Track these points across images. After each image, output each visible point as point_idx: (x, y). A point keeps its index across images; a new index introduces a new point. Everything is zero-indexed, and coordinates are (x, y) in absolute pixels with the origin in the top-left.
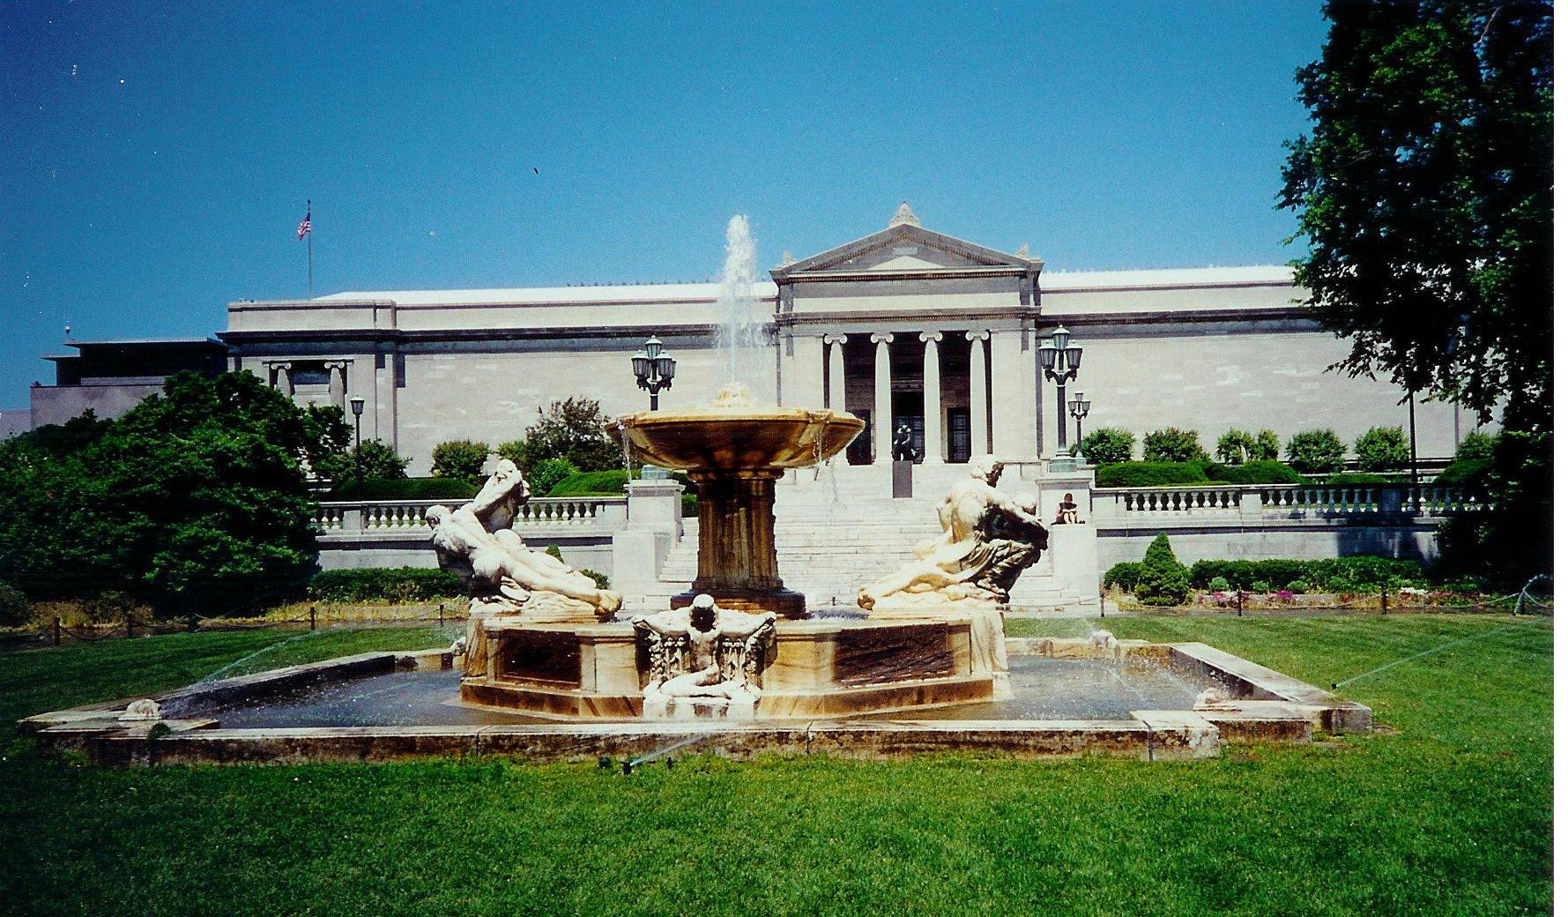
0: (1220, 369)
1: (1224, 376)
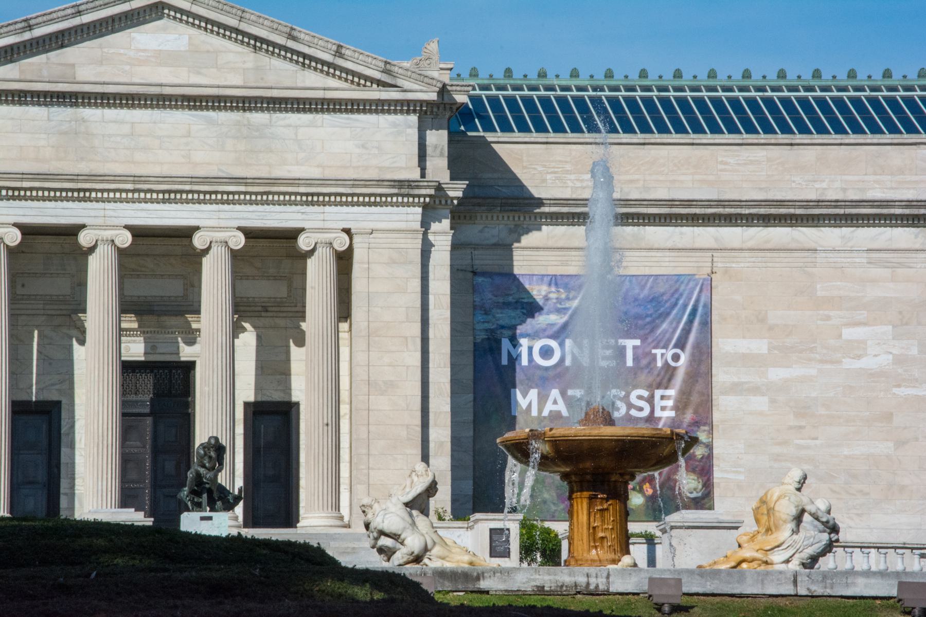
0: (849, 333)
1: (857, 349)
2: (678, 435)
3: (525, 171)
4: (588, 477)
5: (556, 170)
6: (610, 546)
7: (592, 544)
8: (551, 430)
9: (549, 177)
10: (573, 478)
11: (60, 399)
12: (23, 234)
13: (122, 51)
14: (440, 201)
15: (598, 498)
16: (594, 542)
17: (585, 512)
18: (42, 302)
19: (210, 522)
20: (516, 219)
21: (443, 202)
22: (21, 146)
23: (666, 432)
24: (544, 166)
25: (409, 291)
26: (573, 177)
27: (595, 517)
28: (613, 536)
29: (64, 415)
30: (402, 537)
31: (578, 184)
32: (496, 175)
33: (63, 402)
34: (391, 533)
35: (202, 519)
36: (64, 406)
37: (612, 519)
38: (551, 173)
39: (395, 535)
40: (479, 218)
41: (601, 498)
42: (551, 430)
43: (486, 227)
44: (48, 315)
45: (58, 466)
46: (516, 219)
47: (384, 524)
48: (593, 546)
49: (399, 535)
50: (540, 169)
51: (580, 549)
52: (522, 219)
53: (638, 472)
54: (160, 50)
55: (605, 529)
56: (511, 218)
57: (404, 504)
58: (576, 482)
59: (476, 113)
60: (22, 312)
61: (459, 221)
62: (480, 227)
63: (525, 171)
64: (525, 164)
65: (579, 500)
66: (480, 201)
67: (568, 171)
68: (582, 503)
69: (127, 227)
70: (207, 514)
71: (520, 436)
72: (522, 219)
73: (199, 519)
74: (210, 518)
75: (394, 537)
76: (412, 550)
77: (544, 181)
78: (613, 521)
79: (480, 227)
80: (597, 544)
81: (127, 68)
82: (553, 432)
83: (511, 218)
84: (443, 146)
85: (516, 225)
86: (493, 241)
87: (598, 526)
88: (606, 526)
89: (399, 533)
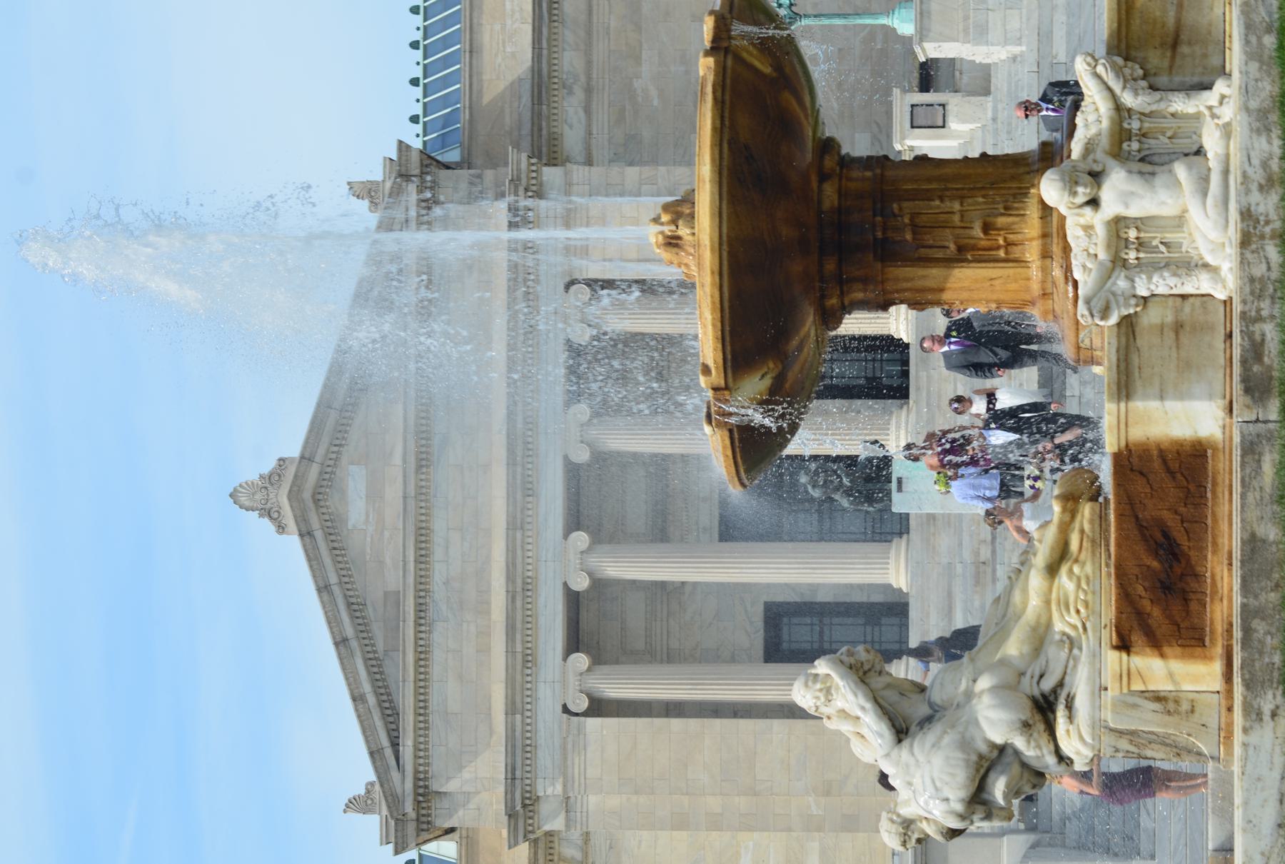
2: (716, 39)
3: (502, 77)
4: (830, 266)
5: (501, 41)
7: (1002, 253)
8: (706, 370)
9: (508, 50)
10: (833, 301)
13: (369, 539)
14: (533, 178)
15: (885, 240)
16: (998, 248)
20: (556, 86)
21: (534, 175)
22: (477, 652)
23: (709, 68)
24: (496, 55)
25: (636, 215)
26: (509, 22)
27: (931, 247)
29: (780, 599)
30: (983, 748)
31: (517, 15)
32: (507, 111)
34: (973, 780)
35: (900, 489)
38: (504, 47)
39: (978, 768)
40: (556, 130)
41: (884, 230)
42: (706, 370)
43: (566, 121)
46: (556, 86)
47: (951, 797)
48: (1007, 253)
49: (981, 757)
50: (499, 60)
52: (556, 80)
53: (815, 132)
54: (367, 497)
55: (962, 221)
56: (556, 93)
58: (842, 294)
59: (443, 128)
60: (665, 642)
61: (559, 153)
62: (566, 128)
63: (502, 77)
64: (494, 77)
66: (536, 129)
67: (502, 28)
68: (897, 280)
69: (566, 536)
70: (894, 485)
71: (724, 447)
72: (556, 80)
74: (900, 481)
75: (982, 771)
76: (1019, 725)
77: (513, 54)
78: (942, 200)
79: (566, 128)
80: (1001, 242)
81: (387, 534)
82: (711, 363)
83: (556, 93)
84: (470, 175)
85: (564, 87)
86: (582, 114)
87: (957, 237)
88: (956, 218)
89: (974, 758)
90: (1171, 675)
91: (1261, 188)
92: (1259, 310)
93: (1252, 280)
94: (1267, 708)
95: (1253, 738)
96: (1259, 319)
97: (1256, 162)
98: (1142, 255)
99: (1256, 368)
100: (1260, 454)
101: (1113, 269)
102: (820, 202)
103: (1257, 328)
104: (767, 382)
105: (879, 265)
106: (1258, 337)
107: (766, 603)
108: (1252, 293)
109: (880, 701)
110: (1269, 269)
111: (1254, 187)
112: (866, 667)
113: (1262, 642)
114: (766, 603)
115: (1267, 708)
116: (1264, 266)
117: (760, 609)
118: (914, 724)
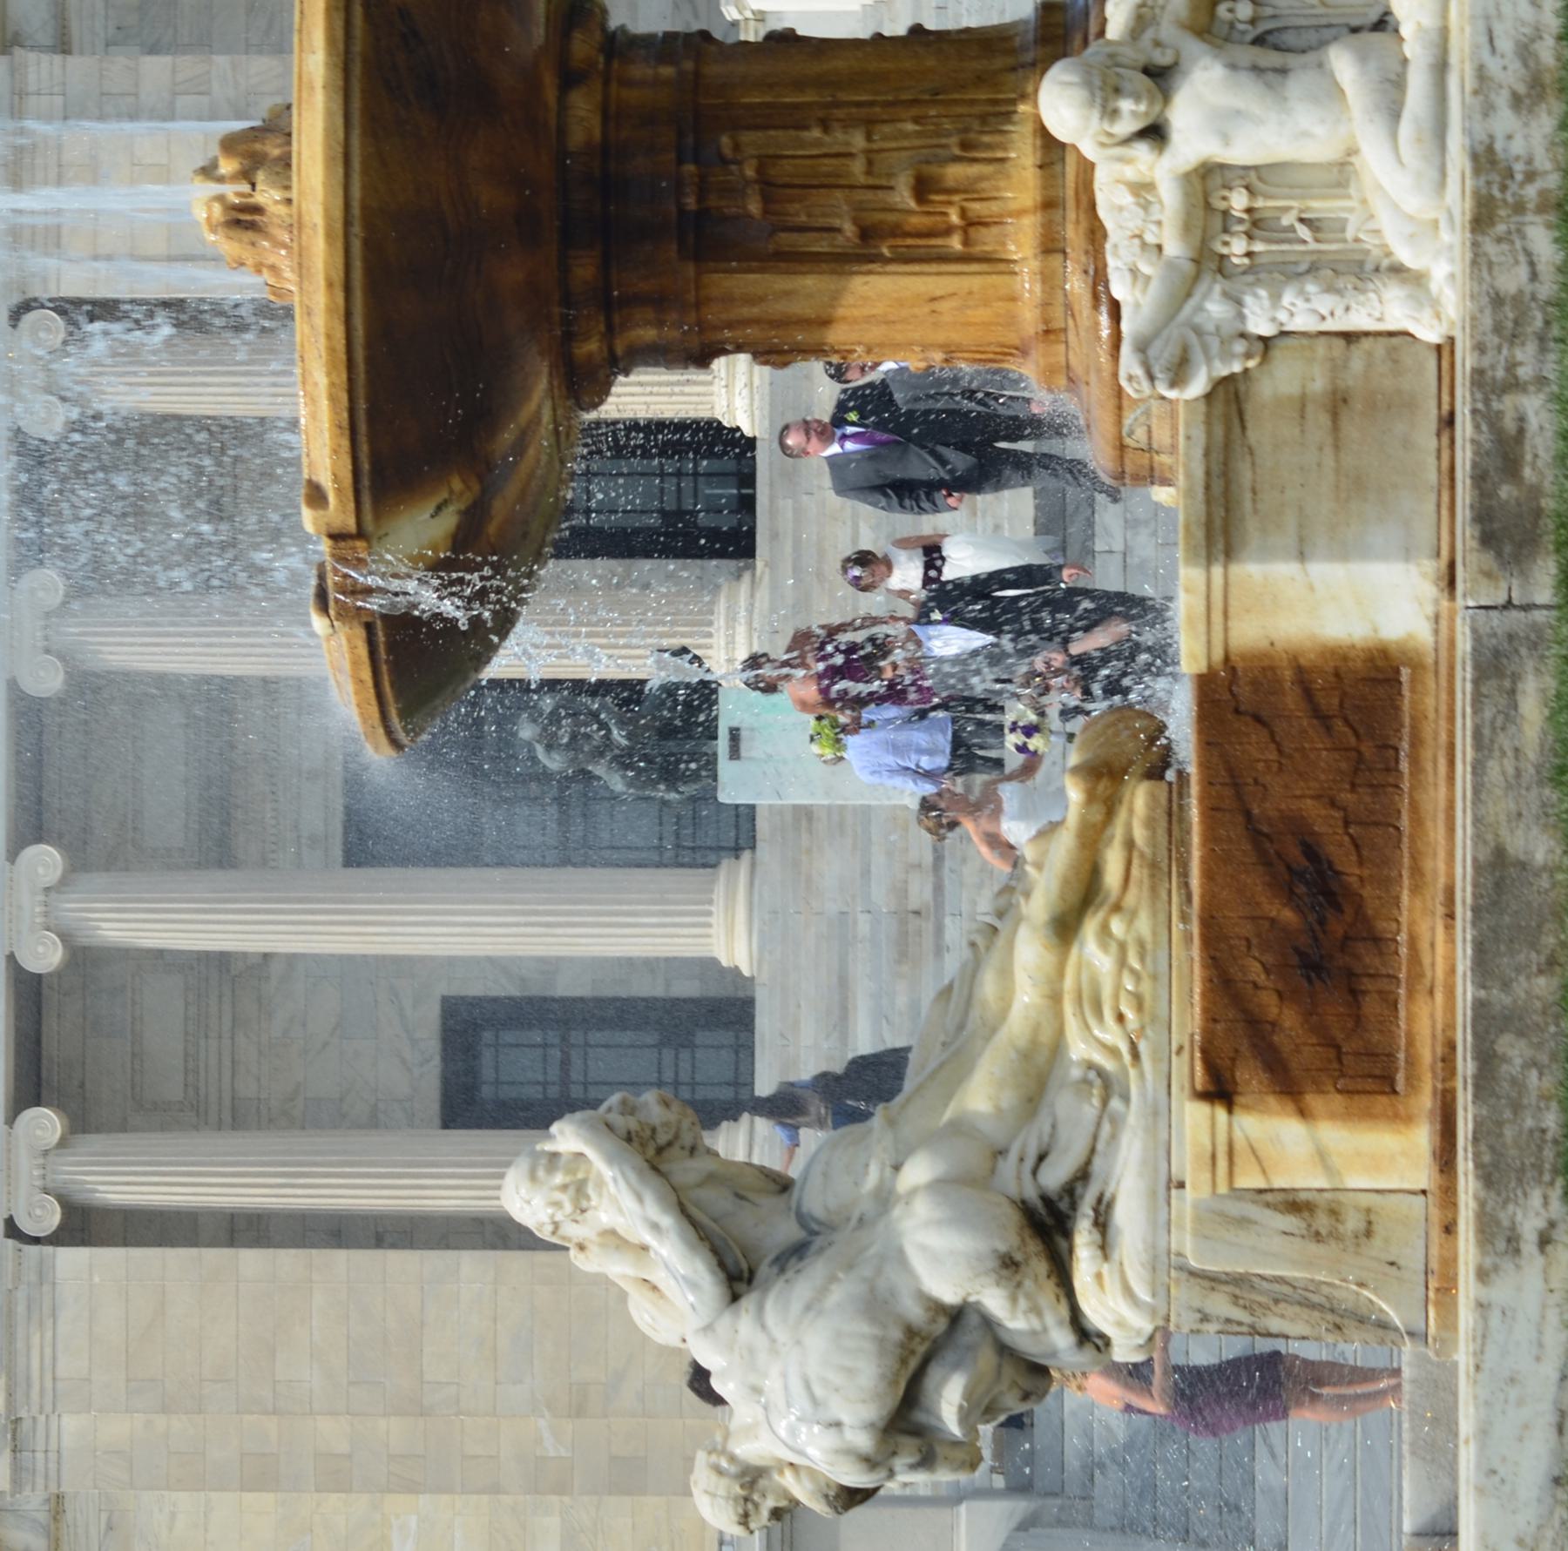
4: (584, 270)
6: (965, 146)
7: (955, 243)
8: (316, 496)
10: (592, 347)
11: (438, 998)
12: (37, 1101)
16: (948, 231)
17: (780, 283)
18: (202, 1042)
19: (744, 734)
28: (910, 127)
29: (475, 990)
30: (915, 1313)
33: (446, 993)
34: (894, 1383)
35: (735, 753)
36: (456, 990)
37: (816, 133)
42: (316, 496)
44: (233, 1027)
45: (600, 1002)
47: (846, 1418)
49: (911, 1332)
51: (981, 314)
55: (869, 173)
57: (735, 1298)
58: (610, 332)
65: (712, 315)
70: (722, 744)
73: (735, 724)
74: (735, 735)
75: (914, 1363)
80: (955, 218)
87: (859, 208)
88: (857, 167)
89: (896, 1334)
90: (1322, 1157)
91: (1517, 101)
92: (1512, 366)
93: (1497, 300)
94: (1530, 1227)
95: (1500, 1292)
96: (1513, 385)
97: (1505, 45)
98: (1258, 247)
99: (1506, 492)
100: (1516, 678)
101: (1197, 278)
102: (562, 131)
103: (1508, 405)
104: (448, 521)
105: (690, 270)
106: (1509, 425)
107: (445, 1000)
108: (1498, 329)
109: (693, 1211)
110: (1534, 276)
111: (1502, 100)
112: (663, 1138)
113: (1518, 1084)
114: (445, 1000)
115: (1530, 1227)
116: (1523, 272)
117: (432, 1013)
118: (767, 1261)
